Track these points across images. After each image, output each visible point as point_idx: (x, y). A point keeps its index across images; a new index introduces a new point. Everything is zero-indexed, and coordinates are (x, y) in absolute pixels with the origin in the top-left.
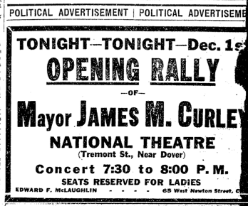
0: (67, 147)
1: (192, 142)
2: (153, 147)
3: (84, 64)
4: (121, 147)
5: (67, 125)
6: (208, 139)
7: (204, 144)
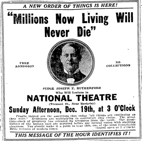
0: (36, 101)
1: (104, 97)
2: (83, 100)
4: (66, 100)
5: (132, 21)
6: (113, 95)
7: (111, 98)
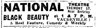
2: (72, 5)
3: (33, 16)
4: (56, 10)
6: (87, 4)
7: (86, 5)
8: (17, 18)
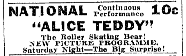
0: (23, 15)
8: (75, 28)
